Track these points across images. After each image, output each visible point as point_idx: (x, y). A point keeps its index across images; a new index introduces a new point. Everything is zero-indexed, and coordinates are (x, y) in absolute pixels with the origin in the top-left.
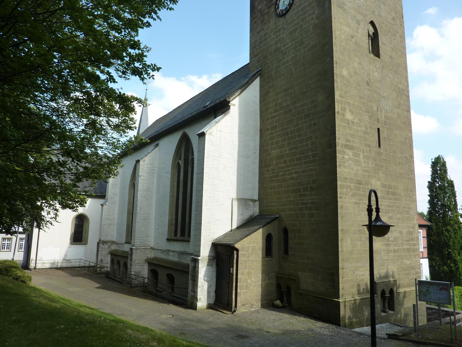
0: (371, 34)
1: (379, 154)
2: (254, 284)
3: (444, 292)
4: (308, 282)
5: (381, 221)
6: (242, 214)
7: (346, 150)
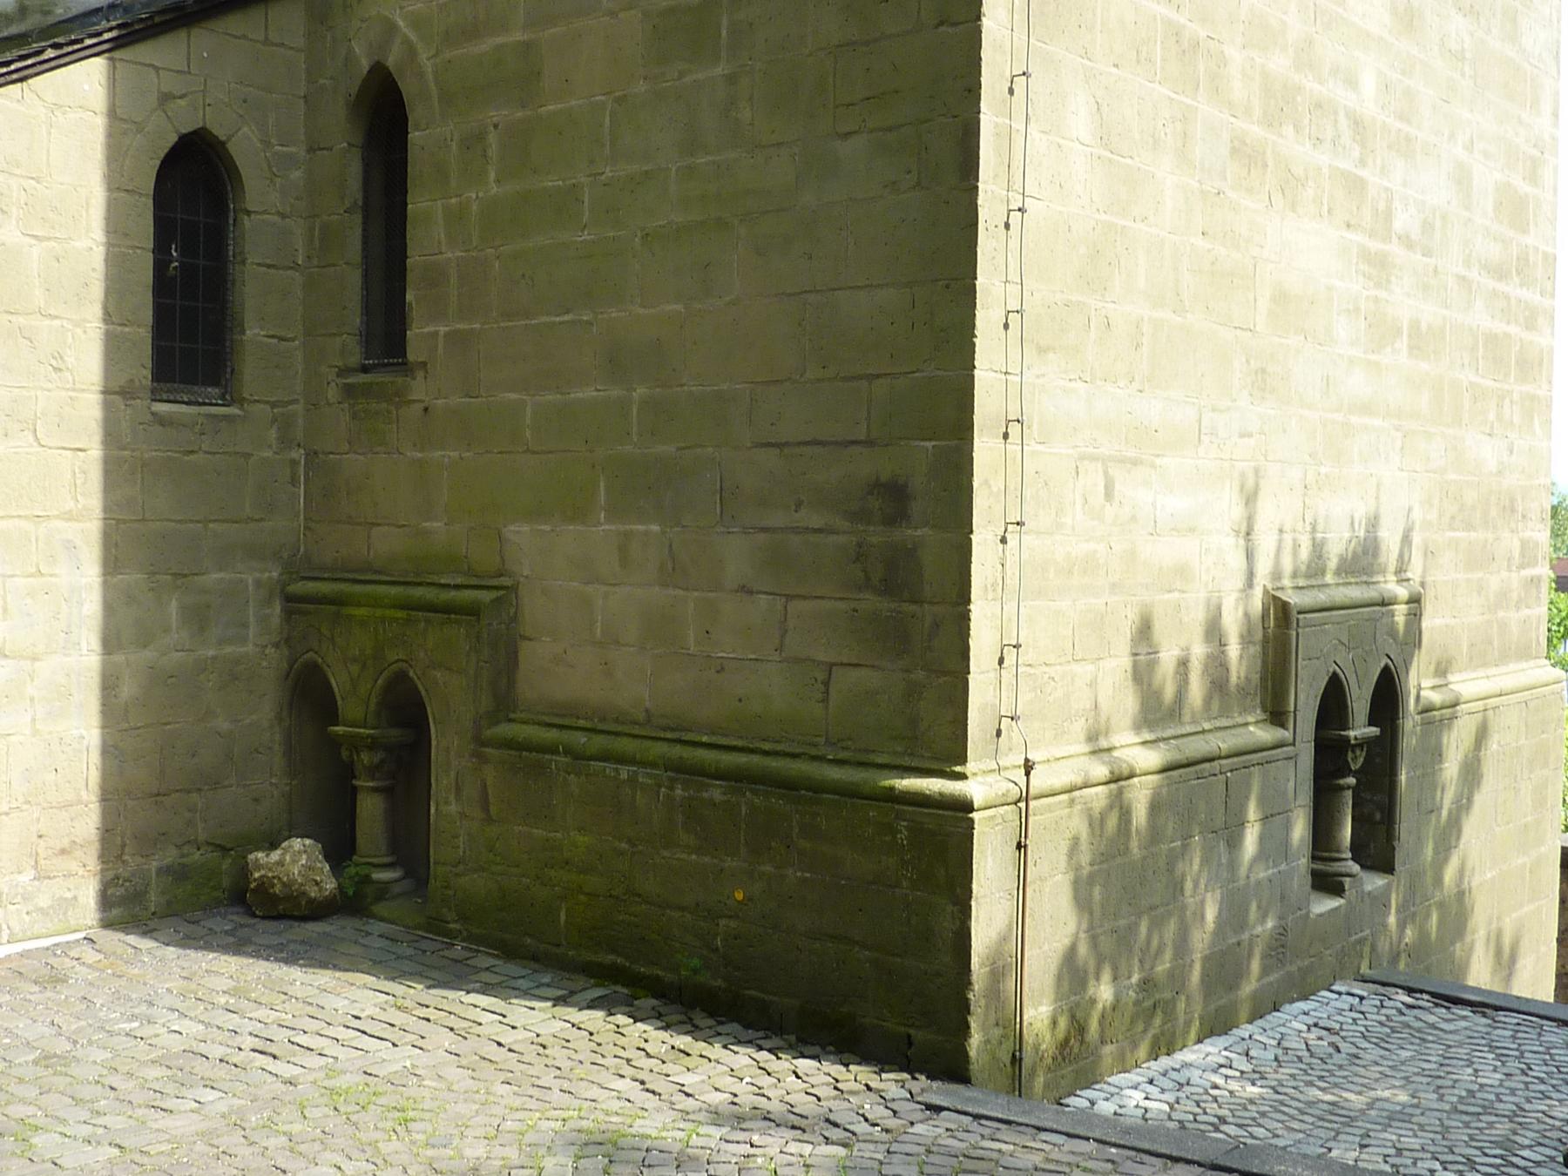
4: (619, 616)
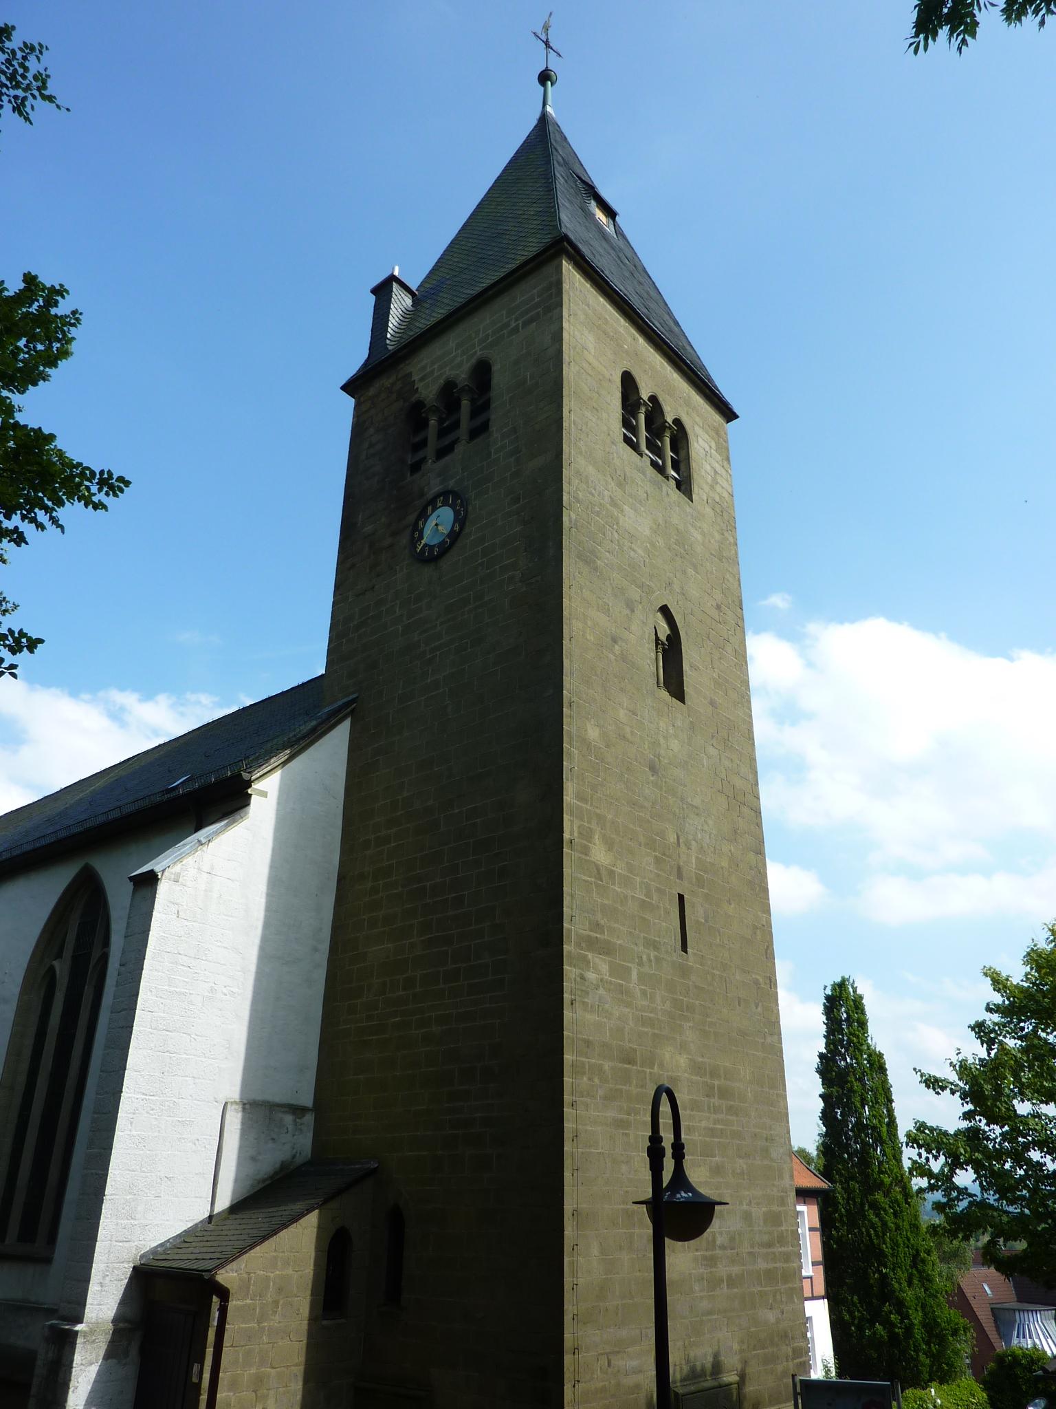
0: (663, 638)
1: (684, 971)
5: (688, 1187)
6: (253, 1159)
7: (590, 955)
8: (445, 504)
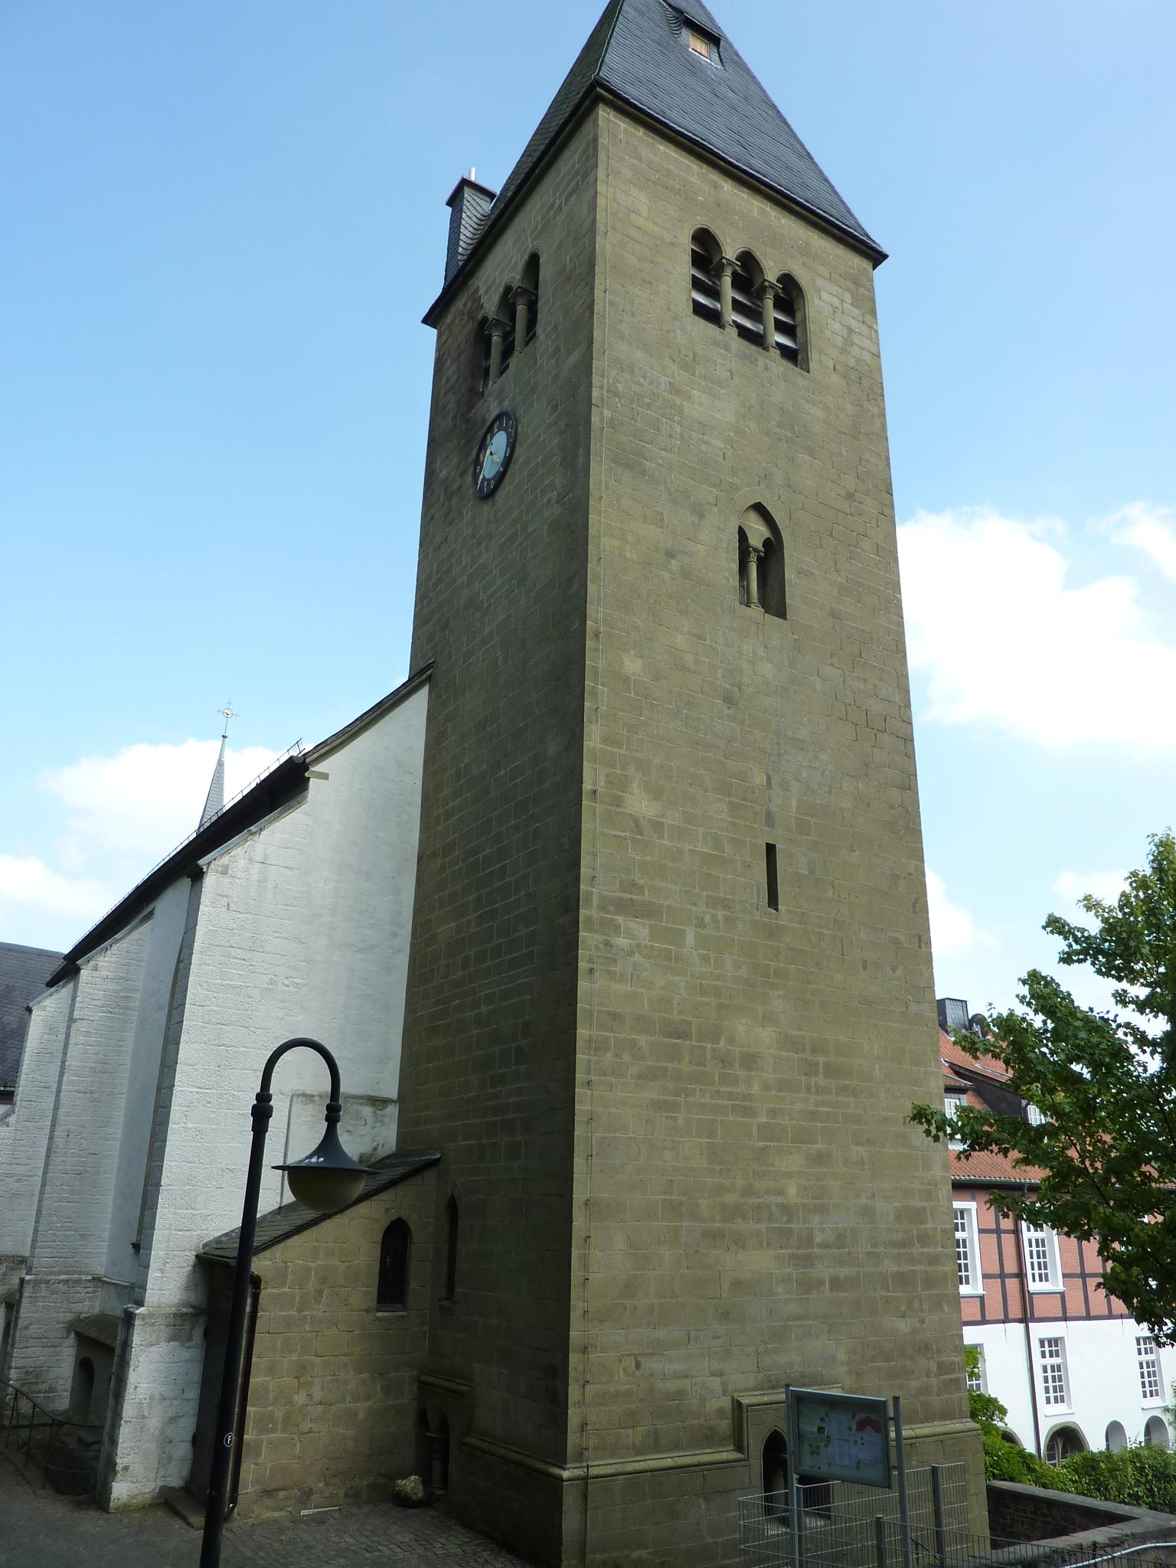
2: (320, 1408)
3: (869, 1435)
7: (620, 919)
8: (500, 429)
